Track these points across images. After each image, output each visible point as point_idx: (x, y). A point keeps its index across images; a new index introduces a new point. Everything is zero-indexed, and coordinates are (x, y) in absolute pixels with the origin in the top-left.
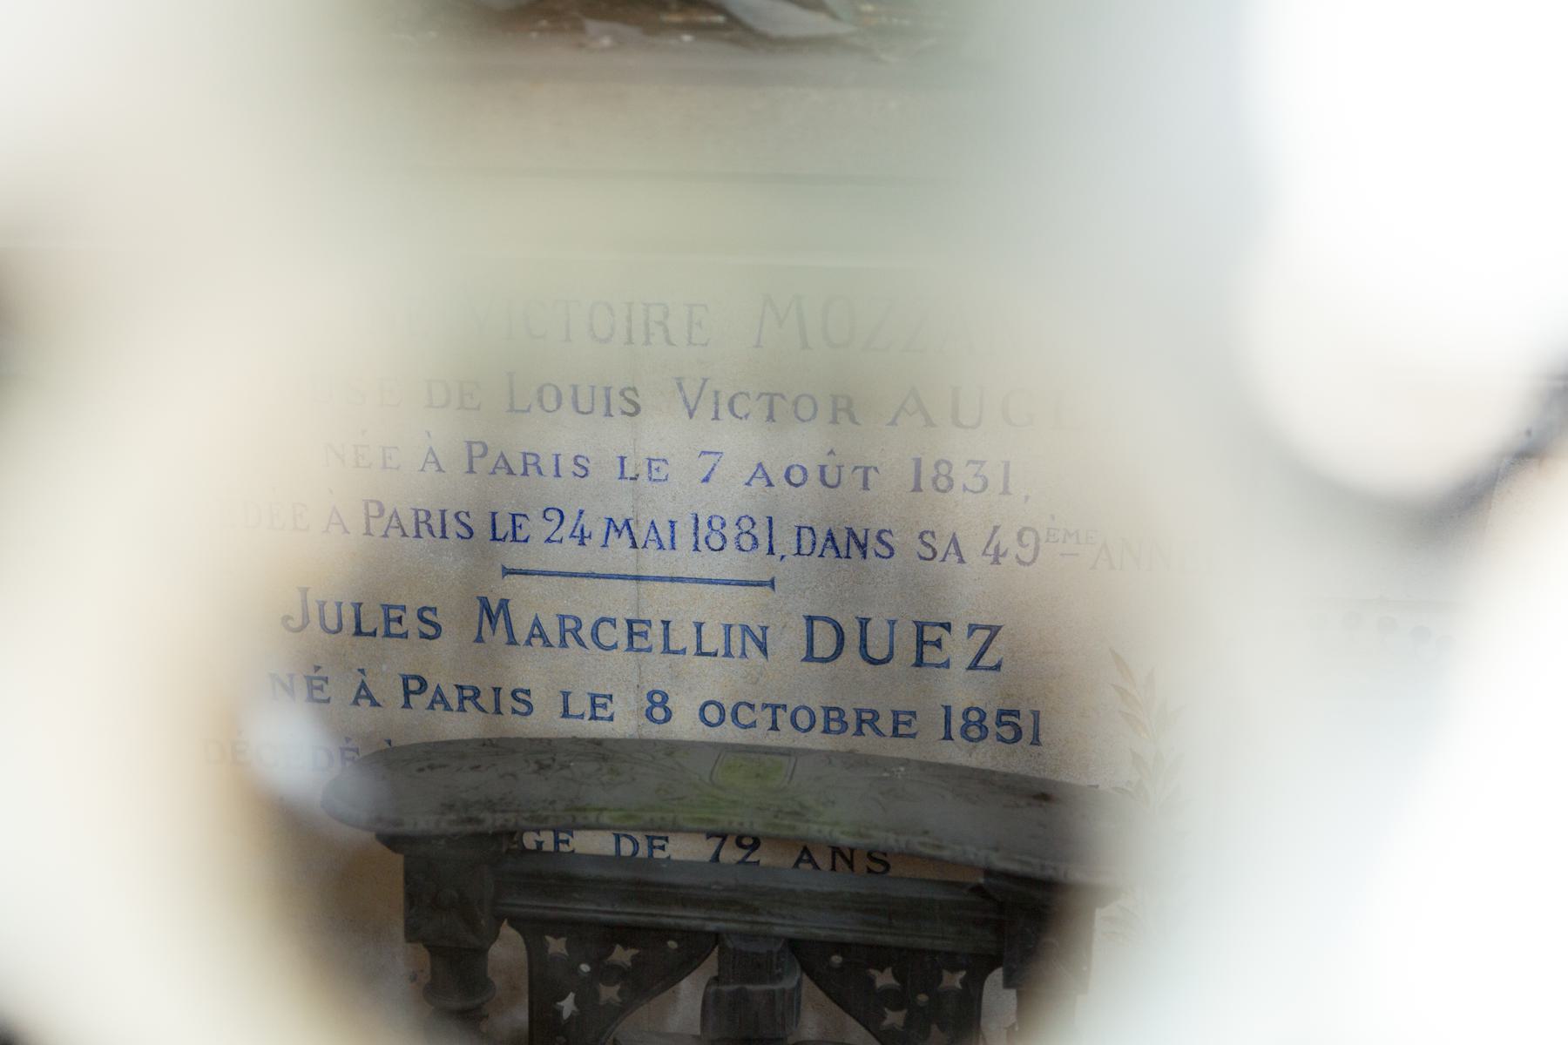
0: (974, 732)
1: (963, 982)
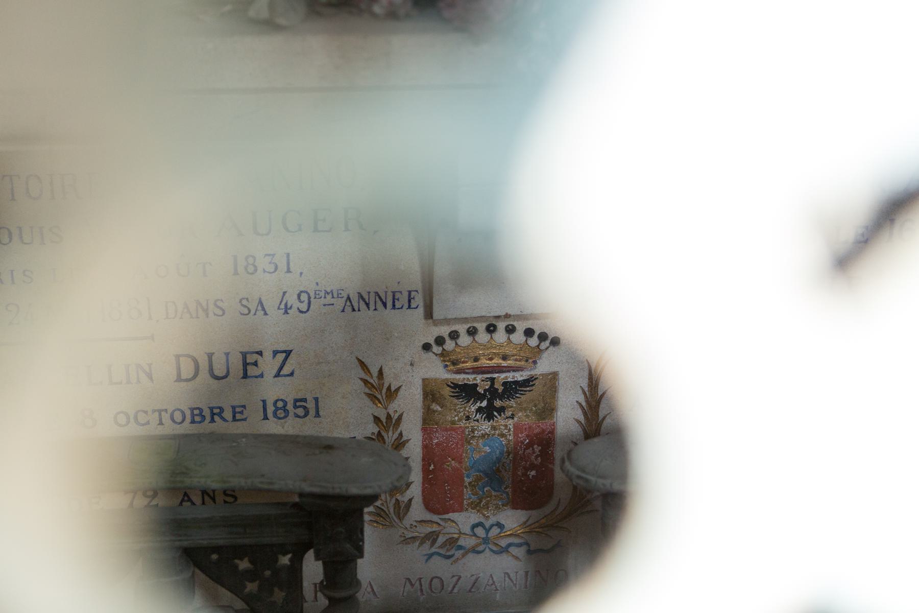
0: (281, 413)
1: (291, 560)
